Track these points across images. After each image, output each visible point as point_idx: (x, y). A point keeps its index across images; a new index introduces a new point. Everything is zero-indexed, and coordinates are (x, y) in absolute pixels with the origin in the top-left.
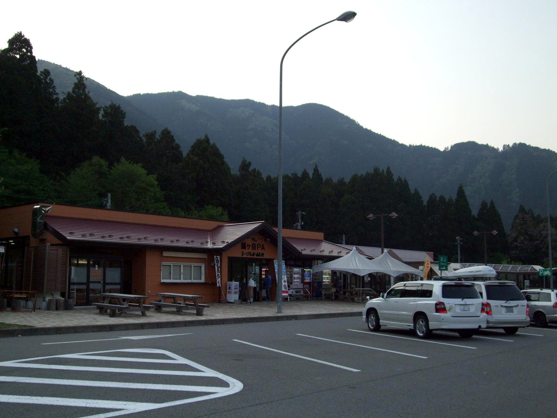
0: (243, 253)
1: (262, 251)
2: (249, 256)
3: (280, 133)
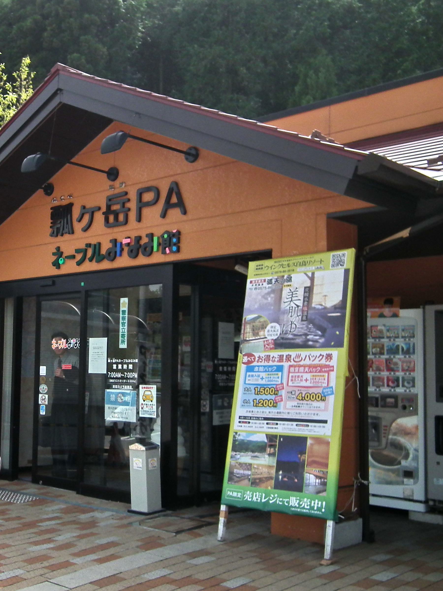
0: (59, 253)
1: (175, 221)
2: (89, 266)
3: (216, 216)
